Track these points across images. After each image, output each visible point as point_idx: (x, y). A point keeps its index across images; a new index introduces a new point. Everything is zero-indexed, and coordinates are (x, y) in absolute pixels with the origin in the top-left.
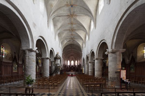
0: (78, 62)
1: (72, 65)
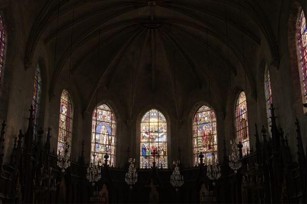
0: (225, 116)
1: (144, 163)
